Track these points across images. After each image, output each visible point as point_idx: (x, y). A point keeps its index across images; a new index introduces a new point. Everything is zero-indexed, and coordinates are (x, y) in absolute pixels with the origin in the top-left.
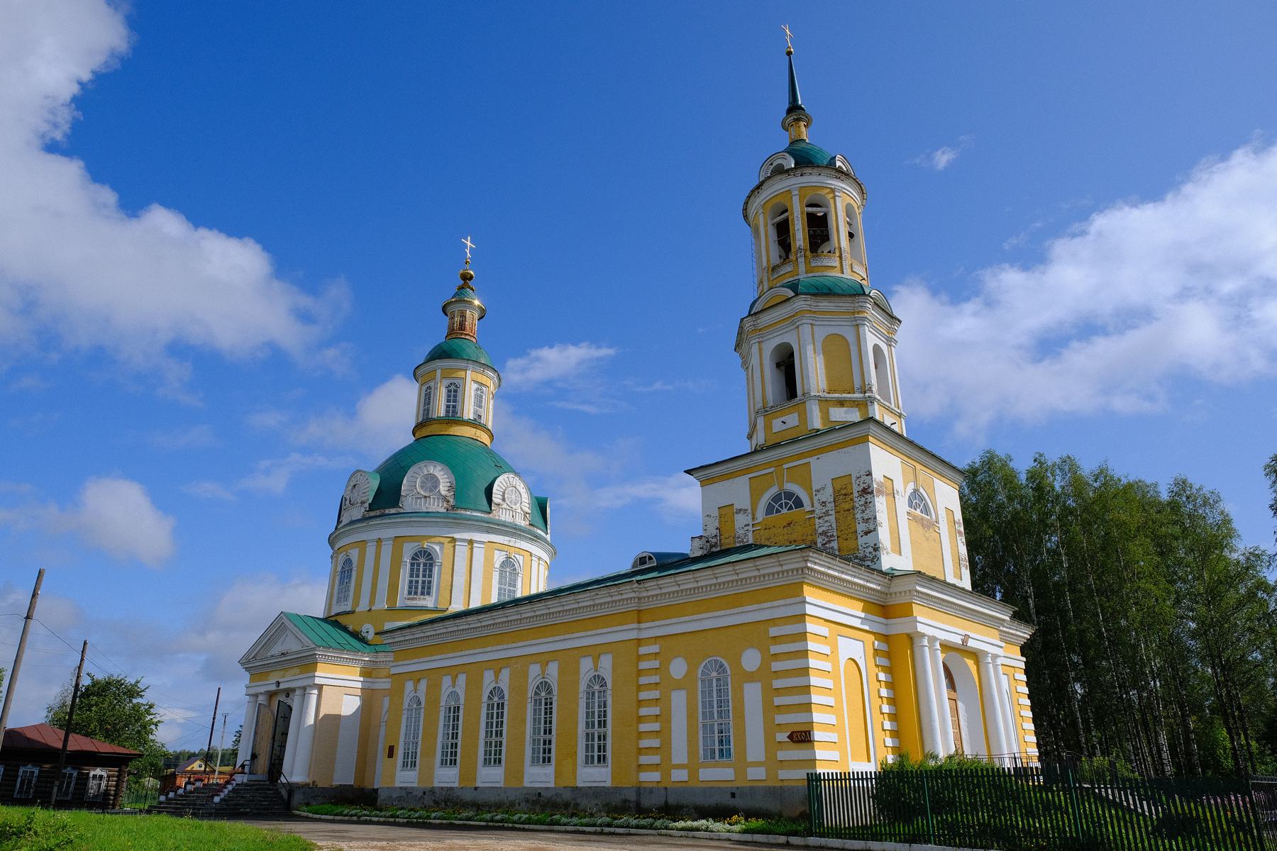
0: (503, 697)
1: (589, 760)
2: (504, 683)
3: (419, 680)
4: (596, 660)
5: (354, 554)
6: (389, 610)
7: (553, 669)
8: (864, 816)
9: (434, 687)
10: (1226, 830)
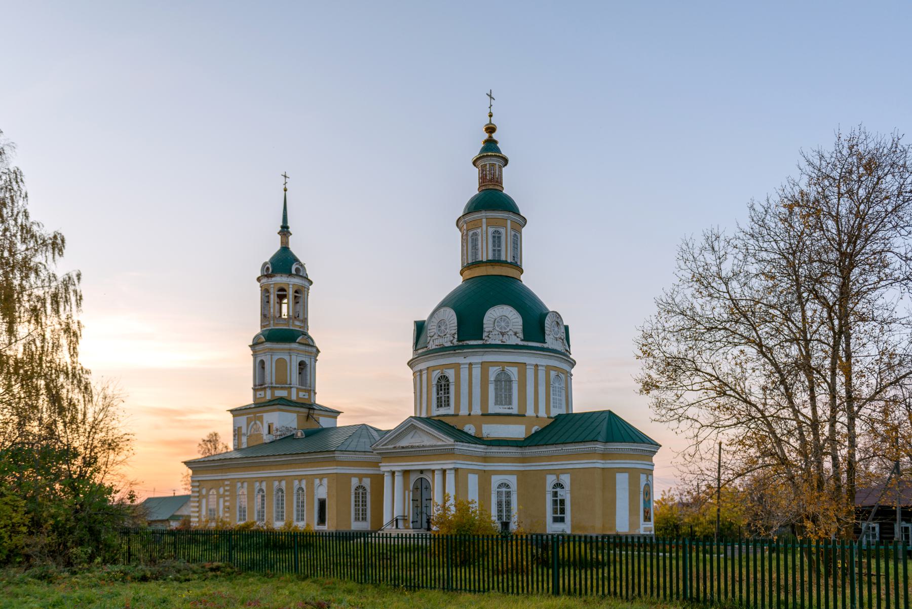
0: (264, 492)
1: (357, 519)
2: (304, 485)
3: (301, 480)
4: (300, 481)
5: (451, 374)
6: (483, 415)
7: (283, 483)
8: (715, 577)
9: (311, 485)
10: (535, 554)
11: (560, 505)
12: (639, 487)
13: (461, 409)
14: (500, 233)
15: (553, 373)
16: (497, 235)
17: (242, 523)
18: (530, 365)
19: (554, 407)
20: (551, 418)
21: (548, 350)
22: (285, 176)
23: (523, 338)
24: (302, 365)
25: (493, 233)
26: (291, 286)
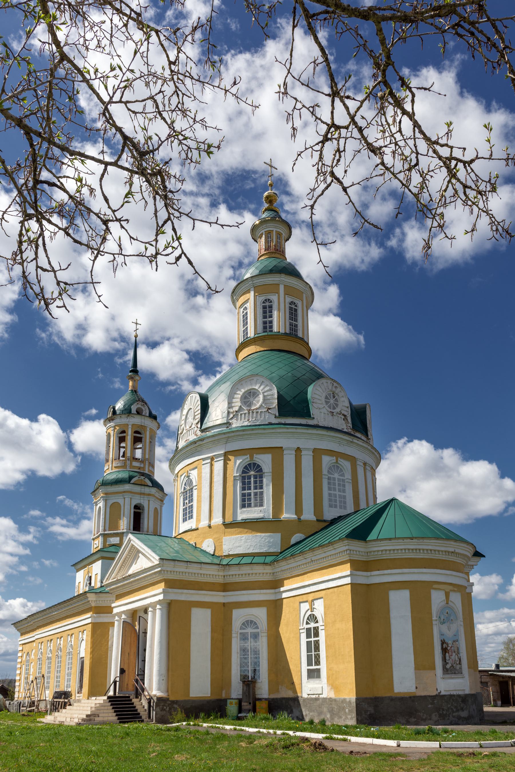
11: (315, 651)
12: (430, 613)
13: (202, 519)
14: (271, 302)
15: (326, 460)
16: (267, 304)
17: (7, 687)
18: (289, 449)
19: (331, 506)
20: (325, 521)
21: (316, 427)
22: (136, 324)
23: (277, 414)
24: (156, 509)
25: (264, 302)
26: (130, 426)
